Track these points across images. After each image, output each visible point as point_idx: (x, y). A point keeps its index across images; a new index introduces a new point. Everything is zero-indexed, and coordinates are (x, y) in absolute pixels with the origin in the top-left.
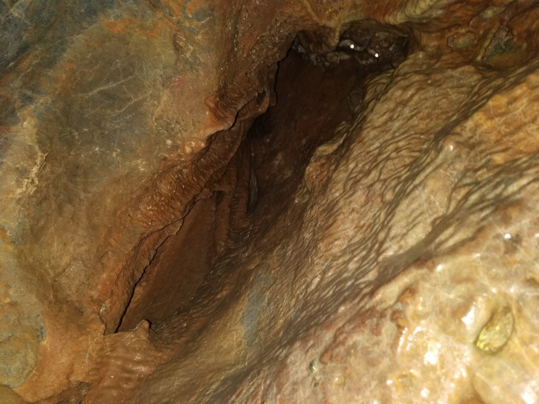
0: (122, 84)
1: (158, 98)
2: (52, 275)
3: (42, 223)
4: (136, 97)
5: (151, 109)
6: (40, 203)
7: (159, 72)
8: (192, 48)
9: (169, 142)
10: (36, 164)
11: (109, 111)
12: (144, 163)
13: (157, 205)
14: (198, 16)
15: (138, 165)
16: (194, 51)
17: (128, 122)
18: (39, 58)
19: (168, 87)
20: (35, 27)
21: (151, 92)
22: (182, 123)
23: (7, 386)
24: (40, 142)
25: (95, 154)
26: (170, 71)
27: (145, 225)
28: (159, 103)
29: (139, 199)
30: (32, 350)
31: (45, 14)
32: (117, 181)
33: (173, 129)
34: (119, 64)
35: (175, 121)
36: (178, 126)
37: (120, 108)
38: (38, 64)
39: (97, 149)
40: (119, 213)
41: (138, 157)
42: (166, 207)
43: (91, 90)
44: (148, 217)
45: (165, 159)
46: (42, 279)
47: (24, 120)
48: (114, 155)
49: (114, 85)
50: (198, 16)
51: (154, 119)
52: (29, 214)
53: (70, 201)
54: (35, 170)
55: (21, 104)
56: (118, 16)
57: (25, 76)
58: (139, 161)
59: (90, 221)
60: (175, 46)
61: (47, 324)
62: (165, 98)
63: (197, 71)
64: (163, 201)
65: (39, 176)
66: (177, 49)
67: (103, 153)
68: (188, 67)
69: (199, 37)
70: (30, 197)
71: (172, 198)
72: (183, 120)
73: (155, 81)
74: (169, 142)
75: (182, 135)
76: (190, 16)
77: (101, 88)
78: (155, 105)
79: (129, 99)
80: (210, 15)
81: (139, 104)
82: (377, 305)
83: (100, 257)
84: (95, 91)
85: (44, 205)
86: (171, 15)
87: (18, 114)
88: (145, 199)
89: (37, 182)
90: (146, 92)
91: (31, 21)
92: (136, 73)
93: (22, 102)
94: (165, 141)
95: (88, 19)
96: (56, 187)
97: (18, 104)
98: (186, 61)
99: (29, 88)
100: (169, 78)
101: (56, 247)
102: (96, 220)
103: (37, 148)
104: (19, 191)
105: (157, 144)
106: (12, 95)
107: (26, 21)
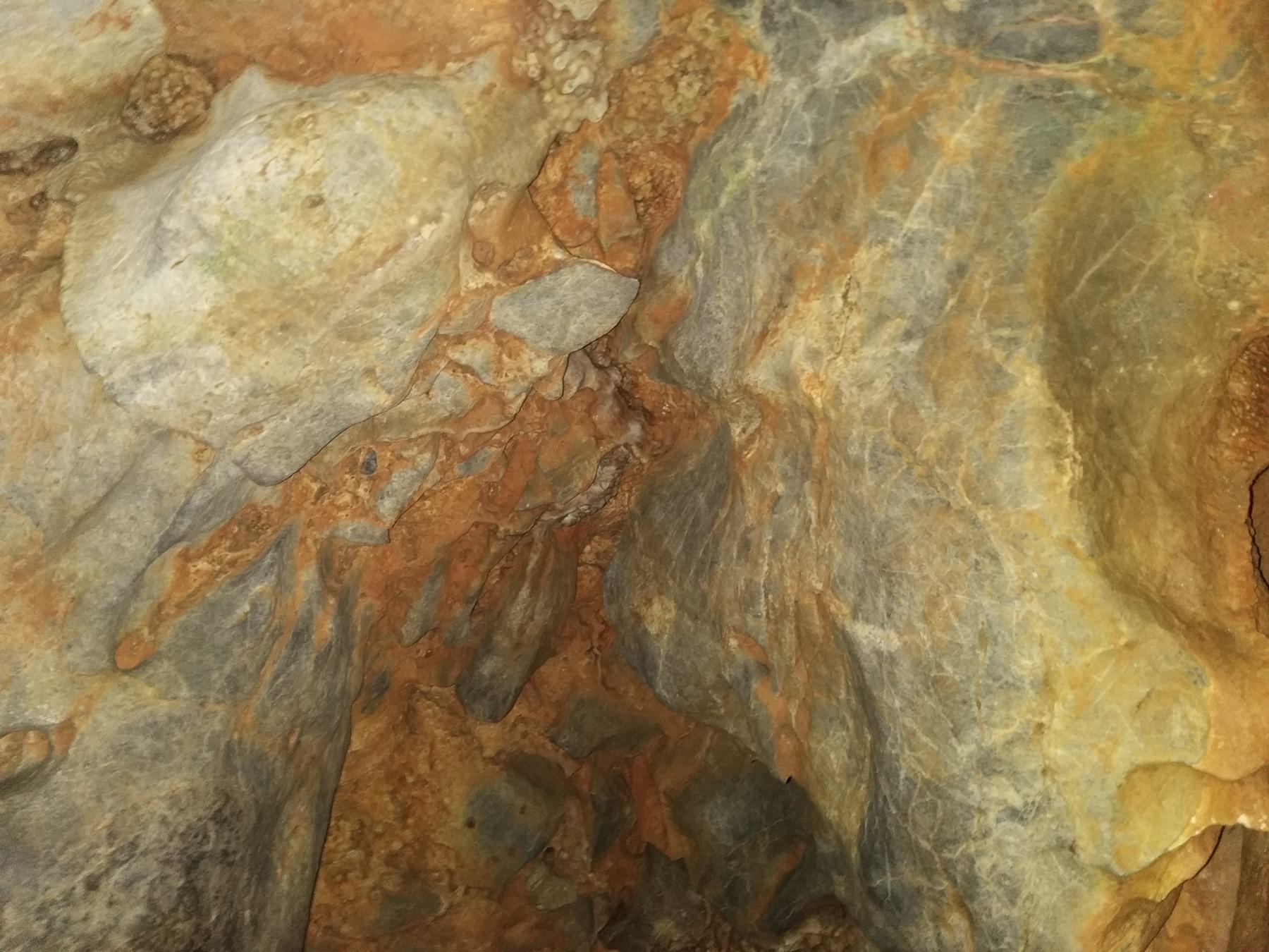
0: (1119, 249)
1: (1191, 241)
2: (1154, 589)
3: (1108, 515)
4: (1149, 257)
5: (1186, 263)
6: (1095, 488)
7: (1176, 197)
8: (1228, 128)
9: (1234, 305)
10: (1067, 431)
11: (1114, 302)
12: (1205, 359)
13: (1244, 422)
14: (1227, 73)
15: (1196, 367)
16: (1236, 130)
17: (1151, 305)
18: (991, 274)
19: (1202, 215)
20: (958, 232)
21: (1173, 237)
22: (1252, 262)
23: (1181, 764)
24: (1058, 398)
25: (1122, 379)
26: (1196, 188)
27: (1244, 464)
28: (1196, 249)
29: (1214, 423)
30: (1193, 706)
31: (963, 206)
32: (1170, 410)
33: (1237, 281)
34: (1105, 219)
35: (1236, 265)
36: (1246, 271)
37: (1129, 288)
38: (995, 283)
39: (1122, 370)
40: (1195, 459)
41: (1191, 355)
42: (1261, 419)
43: (1076, 283)
44: (1242, 450)
45: (1237, 337)
46: (1149, 601)
47: (1024, 374)
48: (1150, 368)
49: (1108, 256)
50: (1227, 73)
51: (1195, 278)
52: (1091, 509)
53: (1126, 469)
54: (1070, 440)
55: (1004, 354)
56: (1086, 149)
57: (985, 310)
58: (1196, 360)
59: (1165, 488)
60: (1193, 140)
61: (1200, 661)
62: (1203, 235)
63: (1251, 159)
64: (1250, 411)
65: (1077, 447)
66: (1200, 143)
67: (1132, 373)
68: (1230, 161)
69: (1241, 102)
70: (1082, 482)
71: (1260, 400)
72: (1252, 257)
73: (1174, 215)
74: (1234, 305)
75: (1259, 282)
76: (1212, 79)
77: (1090, 272)
78: (1188, 255)
79: (1139, 267)
80: (1249, 54)
81: (1160, 268)
82: (102, 671)
83: (1208, 540)
84: (1083, 282)
85: (1101, 487)
86: (1177, 97)
87: (1010, 371)
88: (1223, 421)
89: (1078, 457)
90: (1165, 242)
91: (946, 225)
92: (1138, 219)
93: (1005, 349)
94: (1226, 308)
95: (1041, 179)
96: (1100, 455)
97: (999, 355)
98: (1224, 154)
99: (1003, 326)
100: (1201, 198)
101: (1137, 545)
102: (1172, 485)
103: (1057, 407)
104: (1066, 479)
105: (1216, 318)
106: (982, 345)
107: (937, 229)
